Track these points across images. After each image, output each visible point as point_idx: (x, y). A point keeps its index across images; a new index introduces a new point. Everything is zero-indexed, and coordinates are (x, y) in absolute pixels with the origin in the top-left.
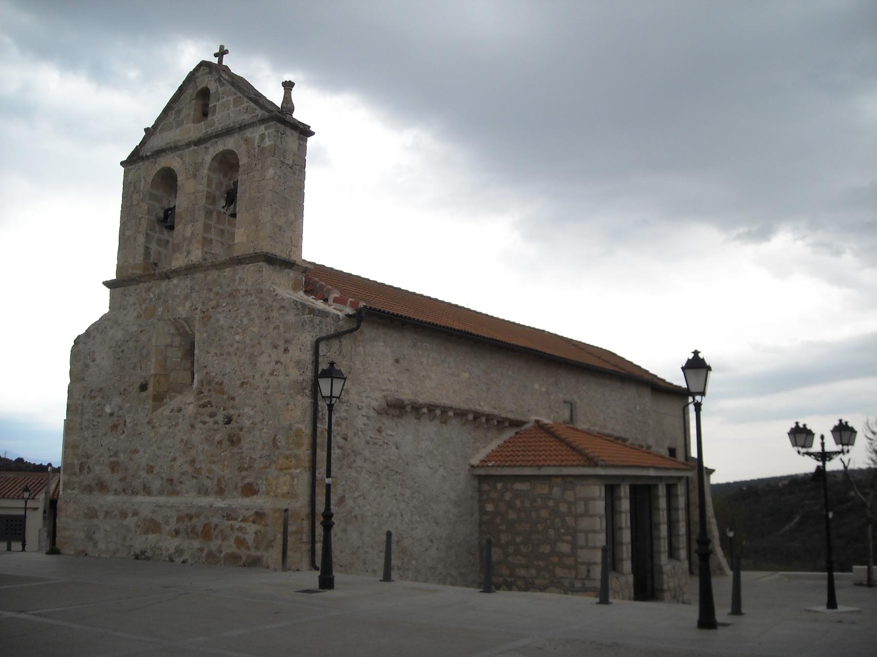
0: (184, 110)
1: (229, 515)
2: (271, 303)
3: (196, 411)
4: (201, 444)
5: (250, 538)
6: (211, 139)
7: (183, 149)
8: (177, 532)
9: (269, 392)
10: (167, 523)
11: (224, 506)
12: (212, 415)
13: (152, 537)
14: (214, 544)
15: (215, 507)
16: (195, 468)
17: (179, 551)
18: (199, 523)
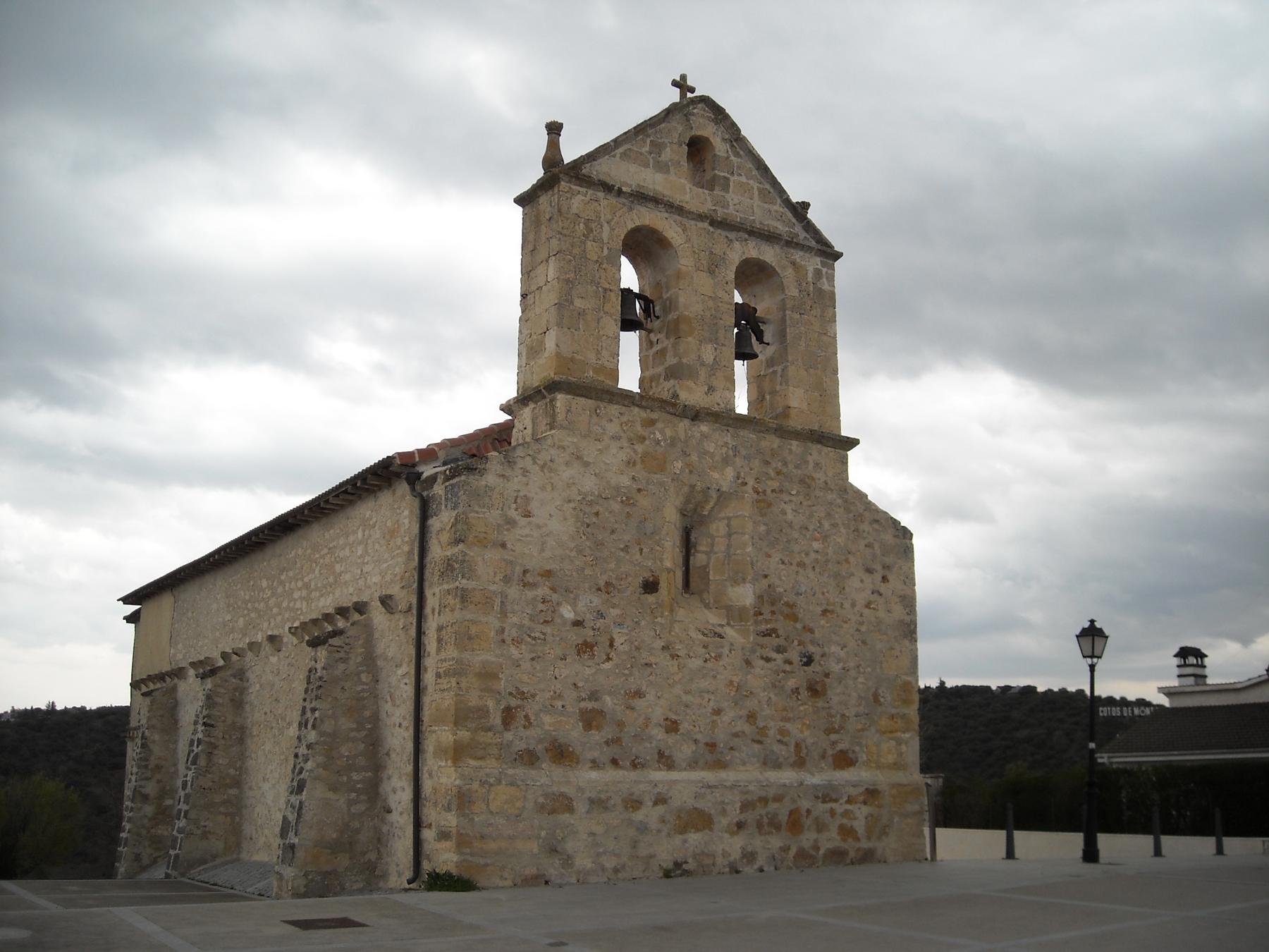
1: (826, 795)
2: (861, 511)
4: (765, 690)
5: (859, 825)
6: (739, 231)
7: (687, 217)
8: (740, 826)
9: (863, 629)
10: (724, 812)
11: (821, 783)
12: (779, 650)
13: (694, 838)
14: (807, 839)
15: (807, 785)
16: (757, 727)
17: (749, 856)
18: (782, 811)
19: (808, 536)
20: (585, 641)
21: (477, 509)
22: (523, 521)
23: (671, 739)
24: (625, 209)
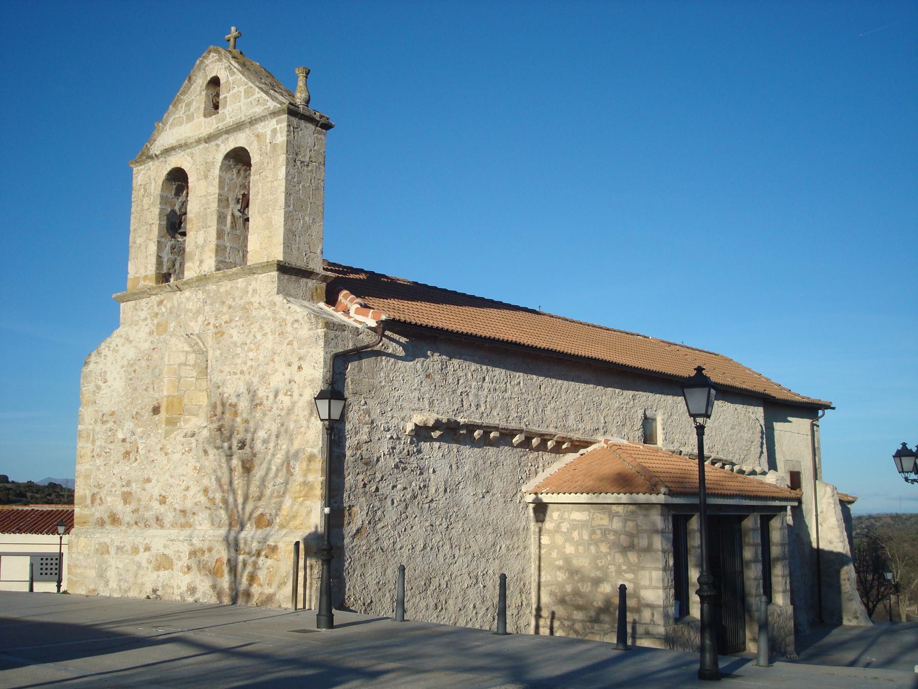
6: (221, 136)
10: (179, 558)
19: (246, 350)
20: (127, 451)
21: (86, 385)
22: (103, 386)
23: (162, 509)
24: (163, 163)
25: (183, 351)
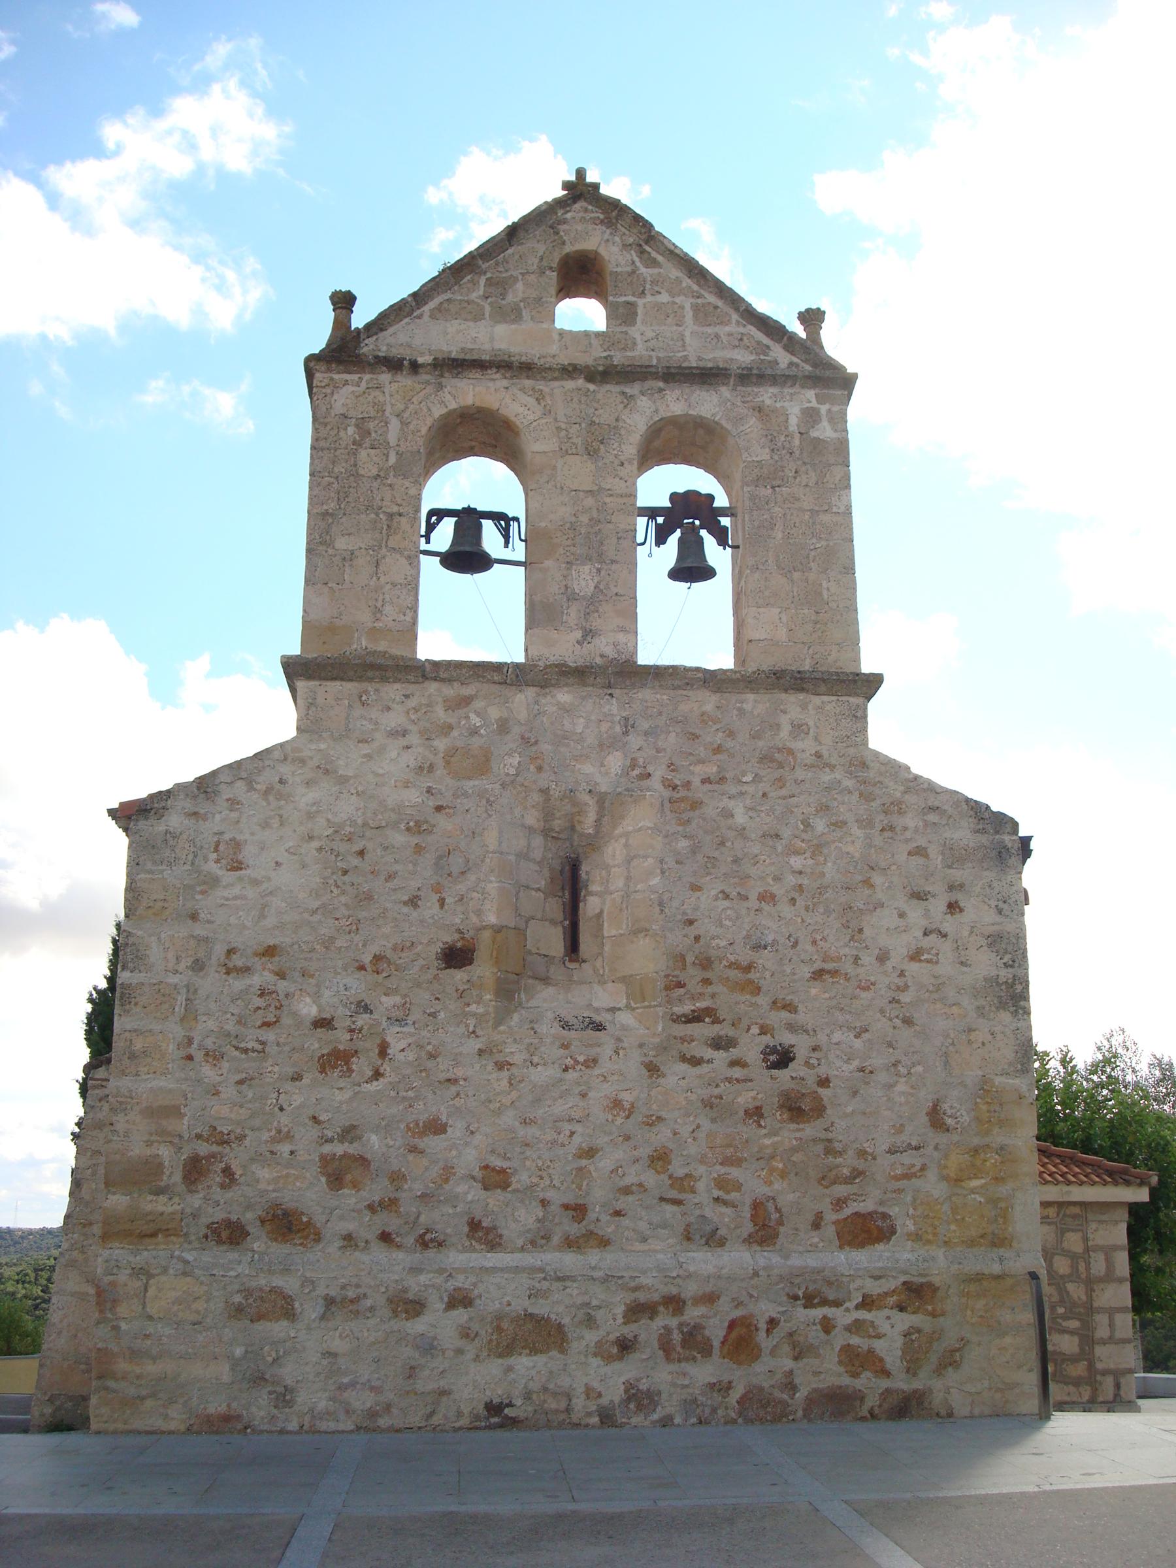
0: (520, 286)
3: (663, 1030)
5: (890, 1349)
9: (906, 998)
10: (590, 1322)
25: (523, 826)
